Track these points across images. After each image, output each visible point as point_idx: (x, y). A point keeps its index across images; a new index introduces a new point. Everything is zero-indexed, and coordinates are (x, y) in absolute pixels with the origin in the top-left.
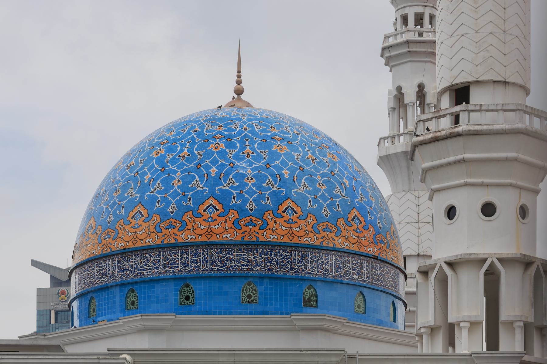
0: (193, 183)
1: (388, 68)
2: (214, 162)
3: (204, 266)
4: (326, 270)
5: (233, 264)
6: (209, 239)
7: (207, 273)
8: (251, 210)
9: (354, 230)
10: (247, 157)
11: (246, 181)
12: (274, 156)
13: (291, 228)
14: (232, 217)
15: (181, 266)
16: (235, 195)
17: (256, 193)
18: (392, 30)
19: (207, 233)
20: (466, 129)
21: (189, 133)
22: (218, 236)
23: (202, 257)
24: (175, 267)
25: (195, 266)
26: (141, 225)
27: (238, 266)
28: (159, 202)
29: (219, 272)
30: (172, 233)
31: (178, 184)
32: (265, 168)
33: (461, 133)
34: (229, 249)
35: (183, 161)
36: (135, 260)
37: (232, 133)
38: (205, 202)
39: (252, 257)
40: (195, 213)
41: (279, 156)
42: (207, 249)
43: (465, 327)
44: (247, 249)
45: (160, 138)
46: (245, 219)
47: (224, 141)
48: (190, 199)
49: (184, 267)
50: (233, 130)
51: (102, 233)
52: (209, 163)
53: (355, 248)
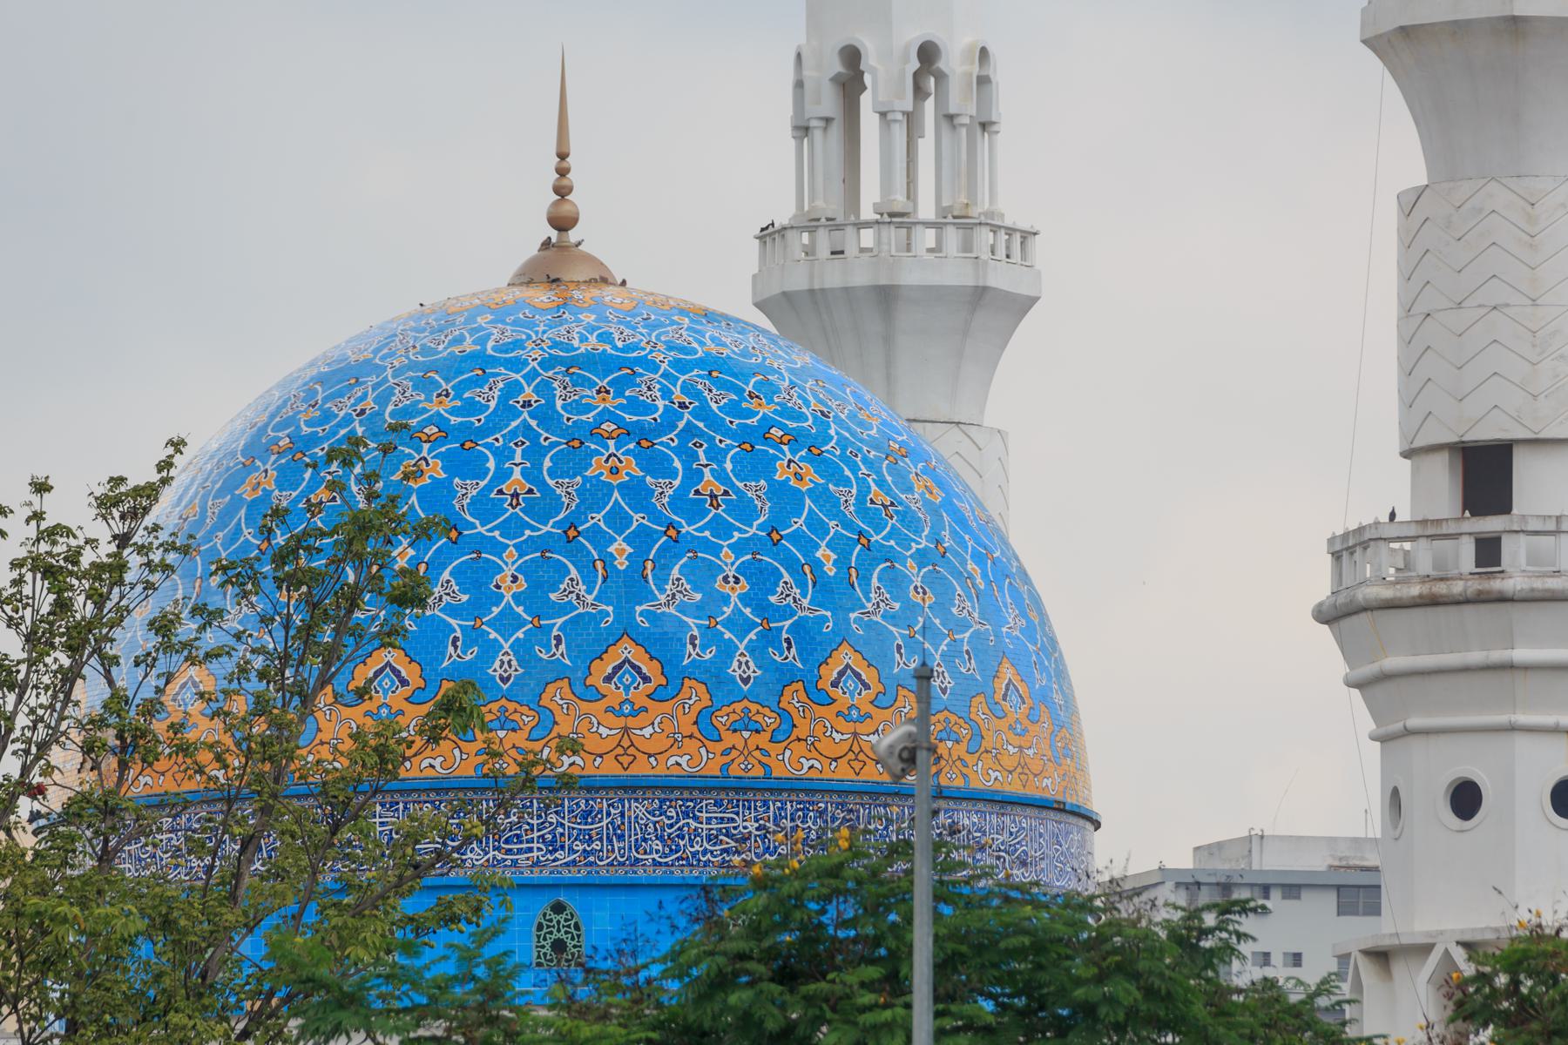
0: (562, 587)
2: (618, 520)
3: (613, 851)
5: (697, 848)
6: (626, 769)
7: (621, 871)
8: (746, 681)
9: (1011, 727)
10: (711, 505)
11: (720, 586)
12: (787, 500)
13: (626, 730)
14: (691, 702)
15: (539, 849)
16: (696, 633)
17: (755, 625)
19: (620, 750)
20: (1525, 586)
22: (652, 759)
23: (605, 822)
24: (520, 851)
25: (585, 850)
27: (712, 852)
28: (459, 644)
29: (659, 871)
31: (514, 590)
32: (769, 543)
33: (1510, 595)
34: (687, 800)
35: (517, 510)
37: (648, 418)
38: (606, 652)
39: (752, 826)
41: (797, 497)
42: (621, 800)
44: (738, 801)
46: (731, 709)
47: (631, 446)
48: (558, 638)
49: (551, 852)
52: (602, 524)
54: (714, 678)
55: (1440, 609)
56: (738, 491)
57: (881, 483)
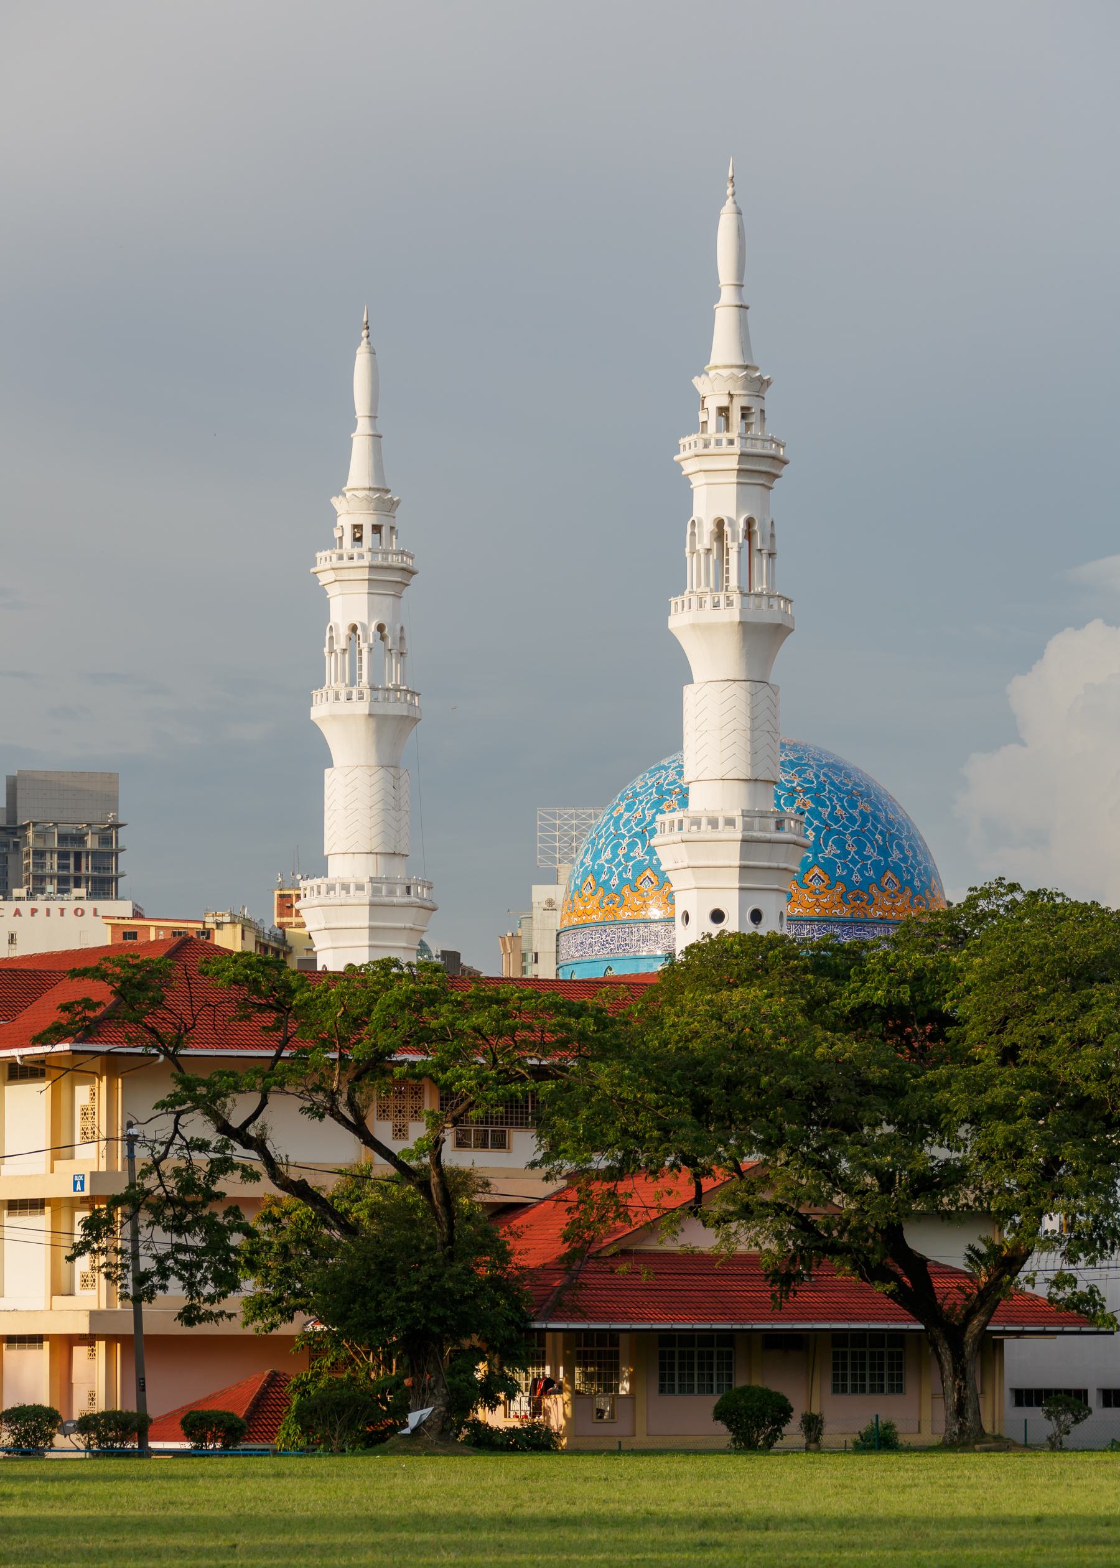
13: (818, 900)
56: (849, 813)
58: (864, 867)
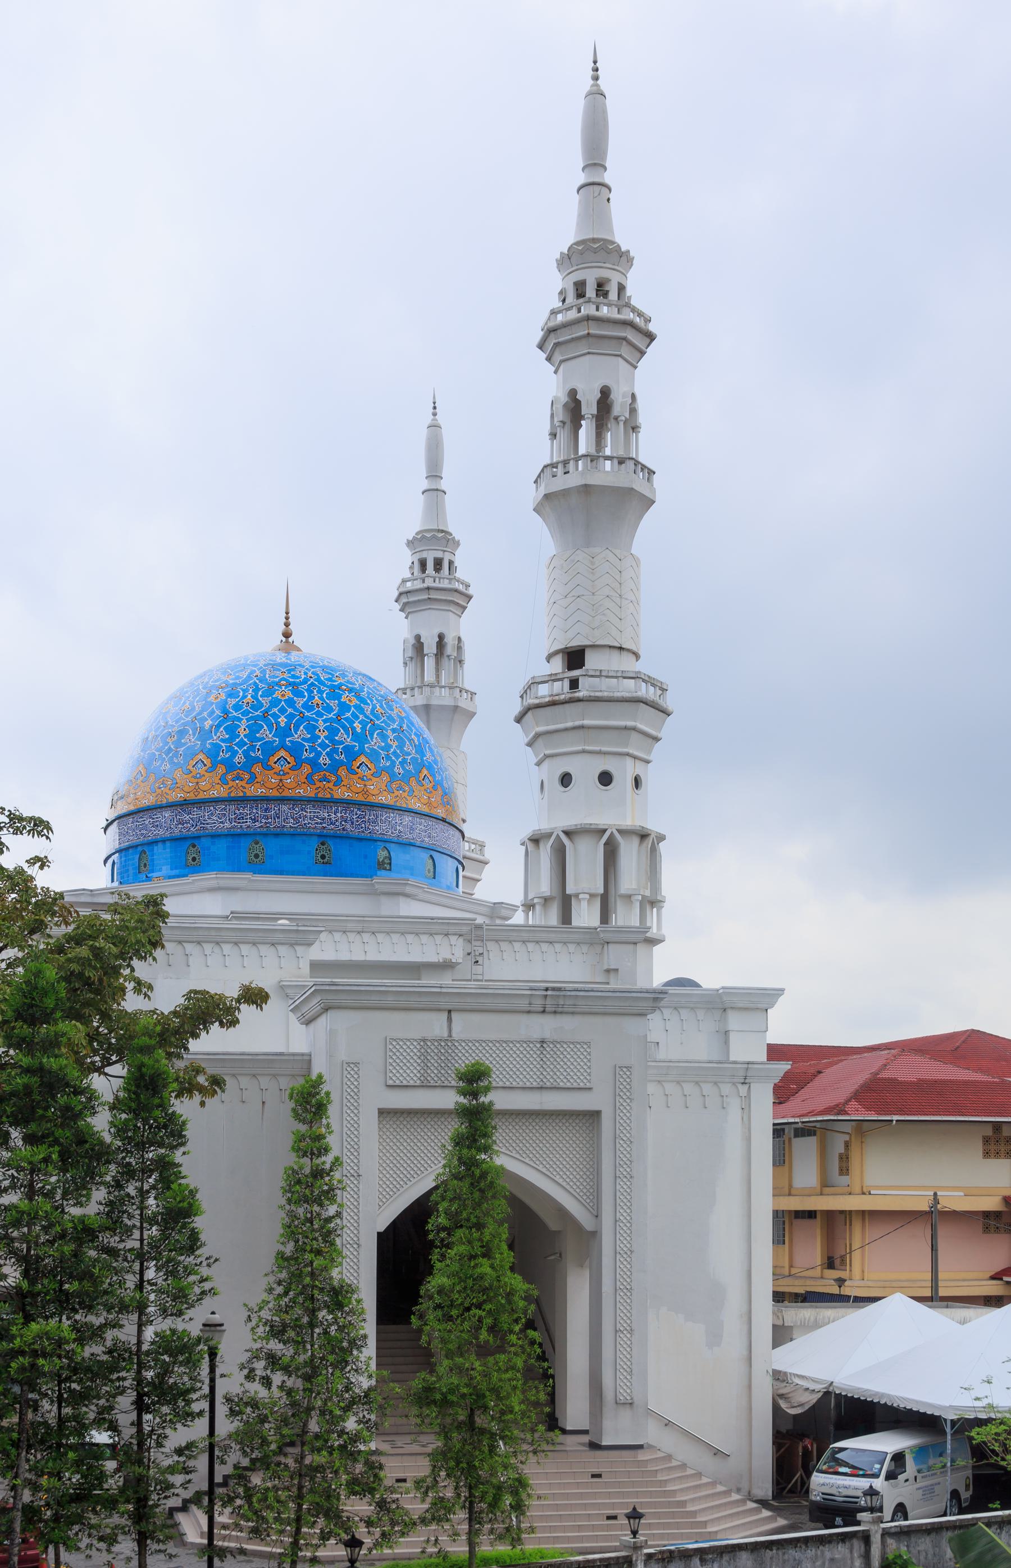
1: (403, 615)
2: (283, 711)
4: (400, 832)
8: (325, 765)
12: (344, 707)
13: (281, 780)
17: (329, 746)
18: (408, 575)
21: (249, 677)
26: (204, 775)
30: (326, 787)
36: (196, 813)
40: (264, 765)
43: (584, 899)
45: (215, 681)
48: (258, 749)
50: (298, 678)
51: (155, 782)
53: (425, 809)
54: (314, 763)
55: (557, 707)
56: (326, 703)
57: (381, 706)
58: (335, 750)
